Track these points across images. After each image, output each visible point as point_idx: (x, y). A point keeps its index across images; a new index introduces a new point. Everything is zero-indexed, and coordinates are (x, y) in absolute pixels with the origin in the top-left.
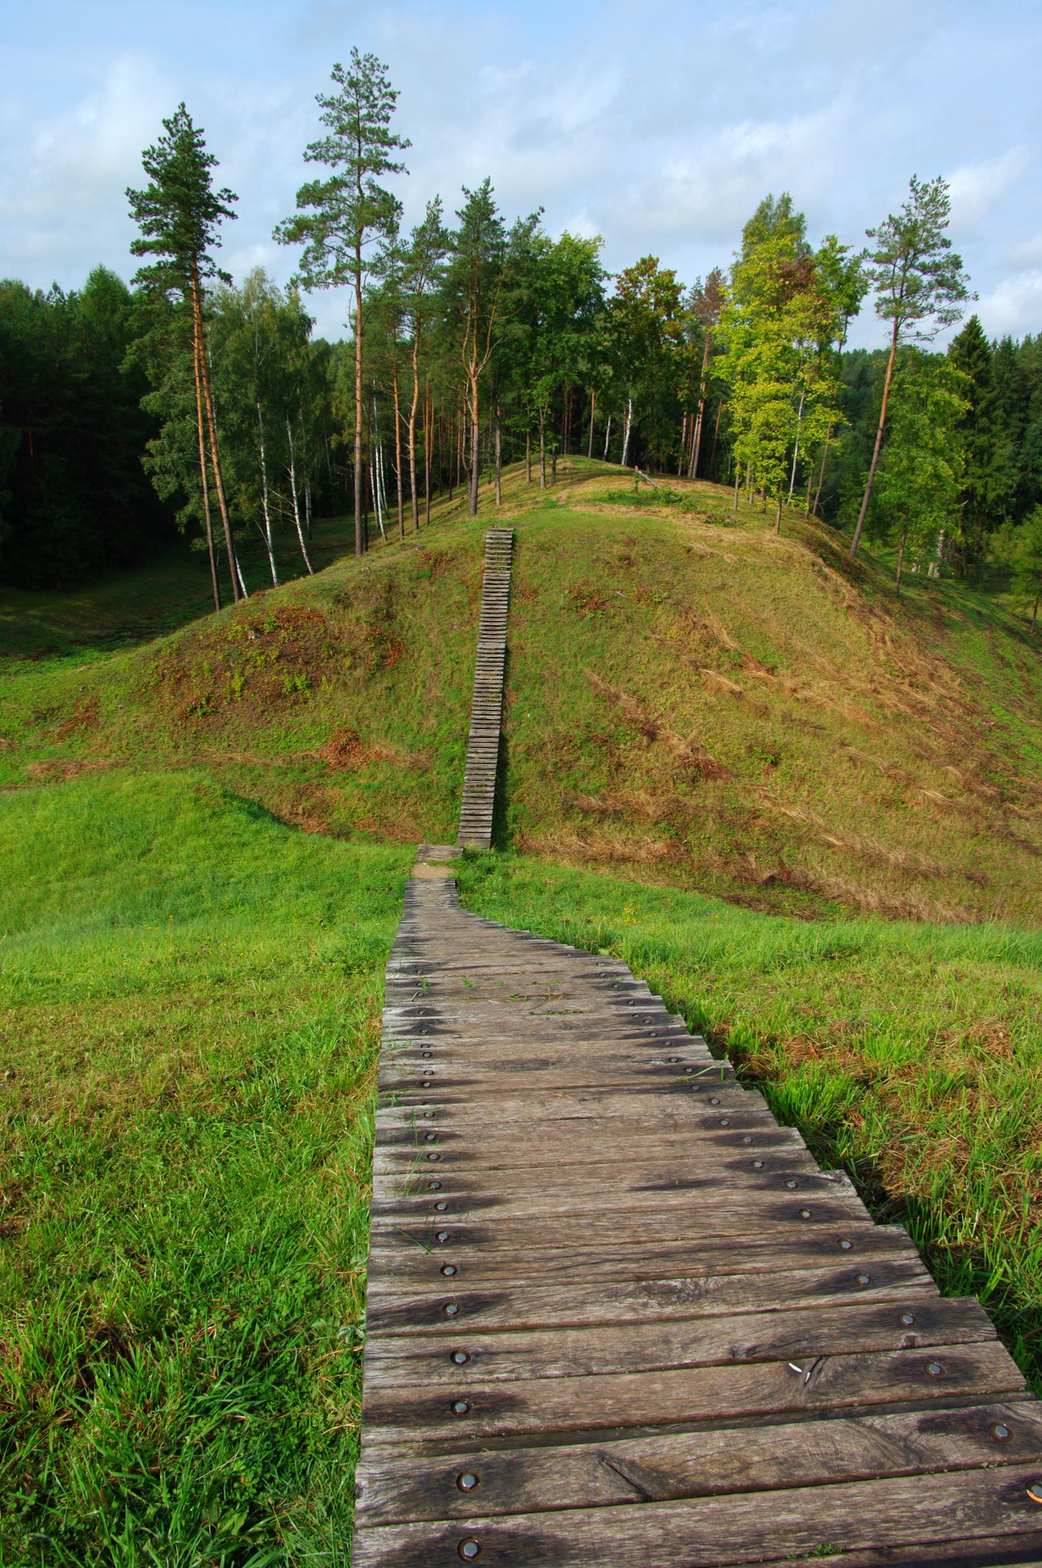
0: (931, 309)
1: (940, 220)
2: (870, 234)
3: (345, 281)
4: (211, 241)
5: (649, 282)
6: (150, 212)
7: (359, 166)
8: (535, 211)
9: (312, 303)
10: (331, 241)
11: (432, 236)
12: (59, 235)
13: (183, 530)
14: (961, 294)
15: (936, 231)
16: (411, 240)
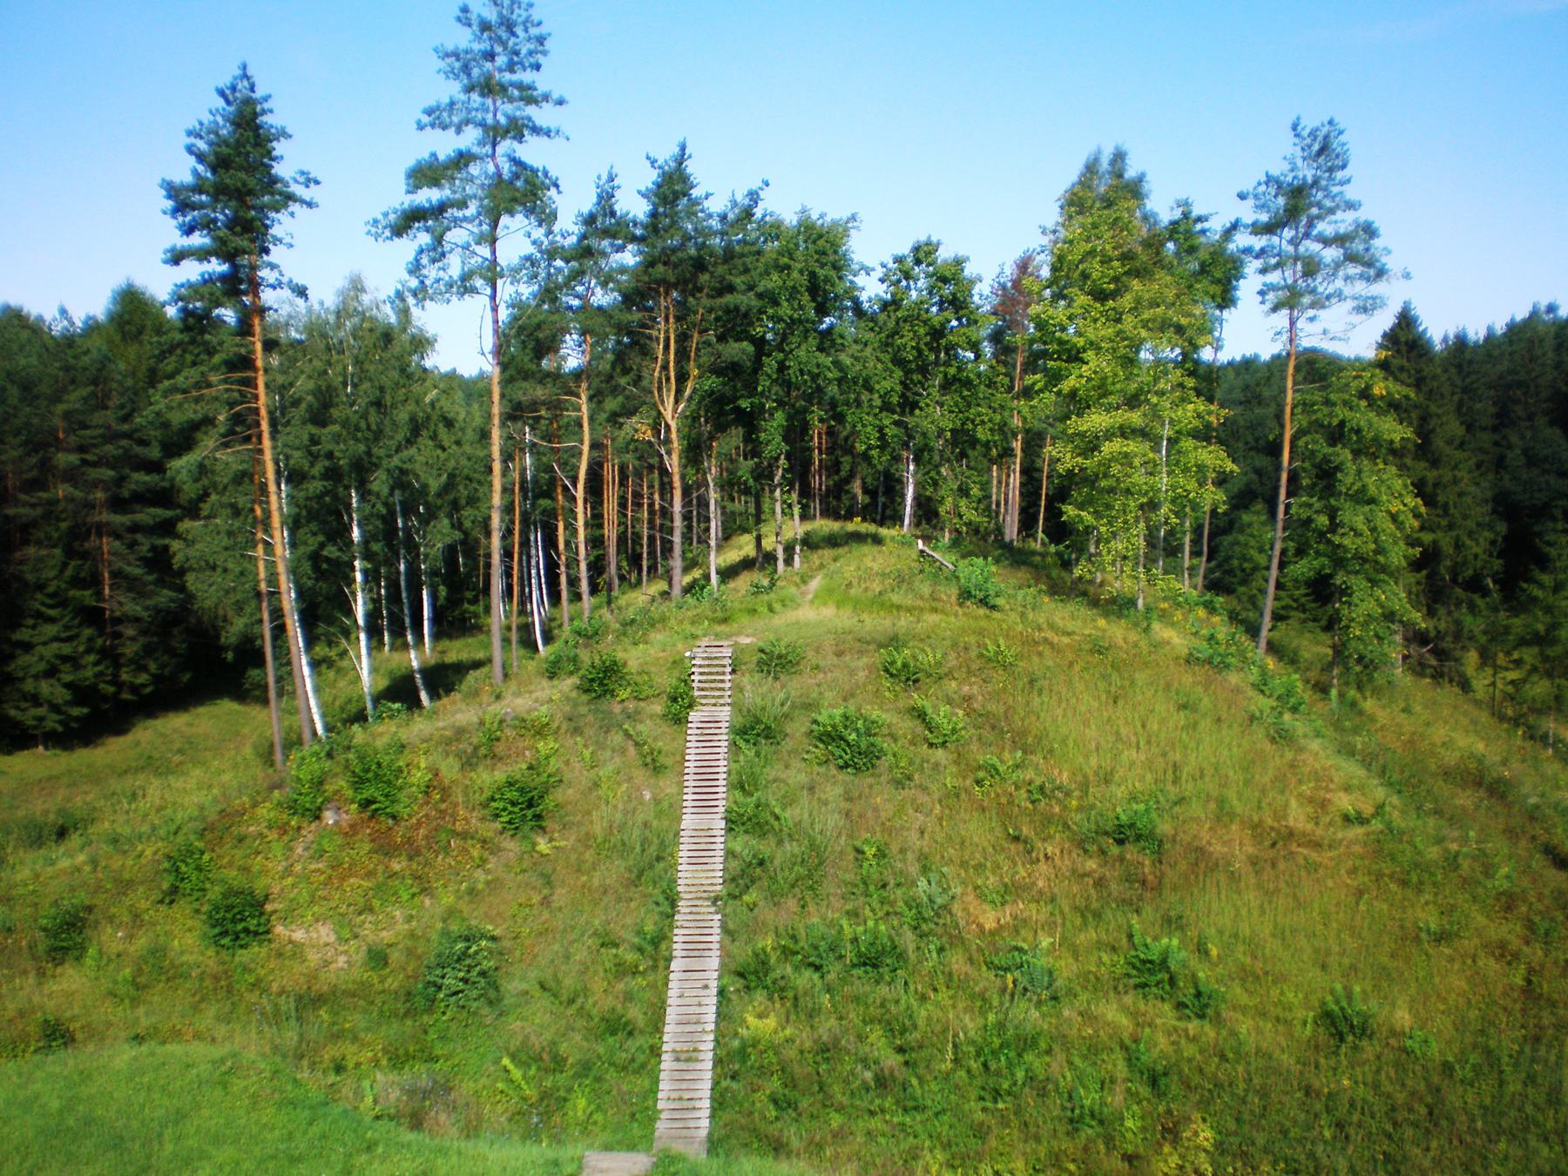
0: (1339, 295)
1: (1339, 175)
2: (1242, 197)
3: (474, 291)
4: (277, 241)
5: (928, 276)
6: (193, 207)
7: (494, 134)
8: (755, 185)
9: (427, 318)
10: (456, 236)
11: (603, 223)
12: (81, 247)
13: (230, 656)
14: (1381, 273)
15: (1335, 190)
16: (577, 229)
